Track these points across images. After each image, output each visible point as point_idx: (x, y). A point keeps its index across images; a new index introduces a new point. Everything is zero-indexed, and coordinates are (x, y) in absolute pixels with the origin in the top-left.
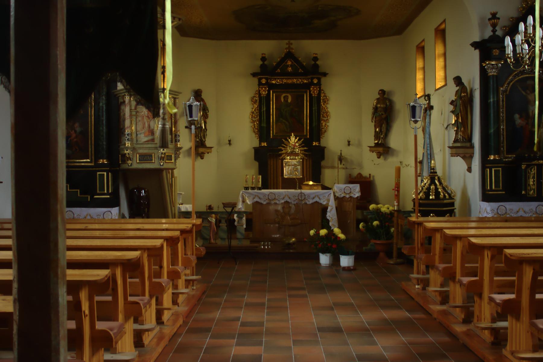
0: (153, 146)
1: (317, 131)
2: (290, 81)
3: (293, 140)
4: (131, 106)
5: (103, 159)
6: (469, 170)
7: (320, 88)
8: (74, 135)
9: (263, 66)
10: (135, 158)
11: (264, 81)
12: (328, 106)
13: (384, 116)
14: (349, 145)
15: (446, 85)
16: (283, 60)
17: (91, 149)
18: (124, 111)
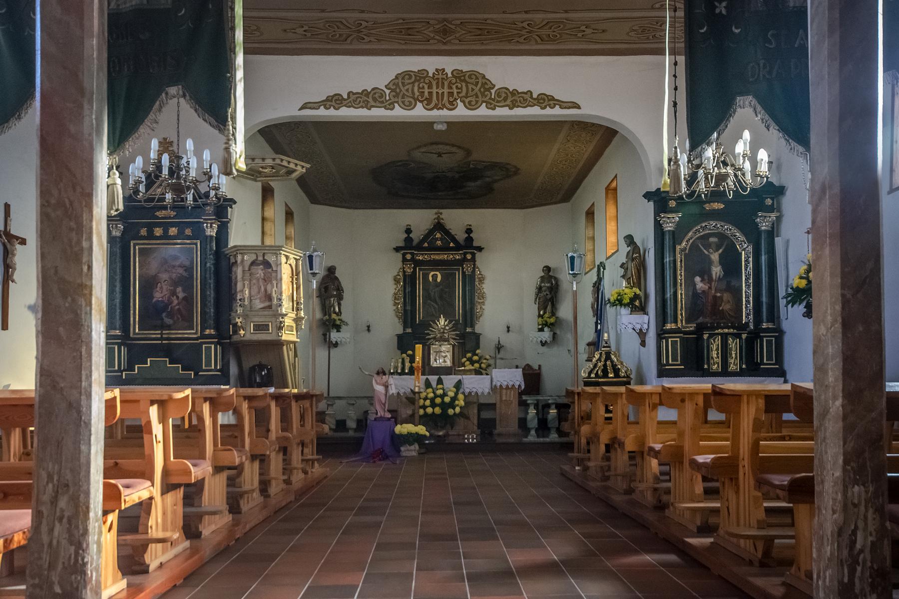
0: (271, 313)
1: (470, 316)
2: (441, 257)
3: (442, 322)
4: (243, 267)
5: (210, 329)
6: (643, 344)
7: (474, 265)
8: (176, 302)
9: (408, 240)
10: (248, 328)
11: (409, 257)
12: (484, 286)
13: (549, 296)
14: (508, 331)
15: (618, 251)
16: (431, 232)
17: (197, 319)
18: (236, 273)
